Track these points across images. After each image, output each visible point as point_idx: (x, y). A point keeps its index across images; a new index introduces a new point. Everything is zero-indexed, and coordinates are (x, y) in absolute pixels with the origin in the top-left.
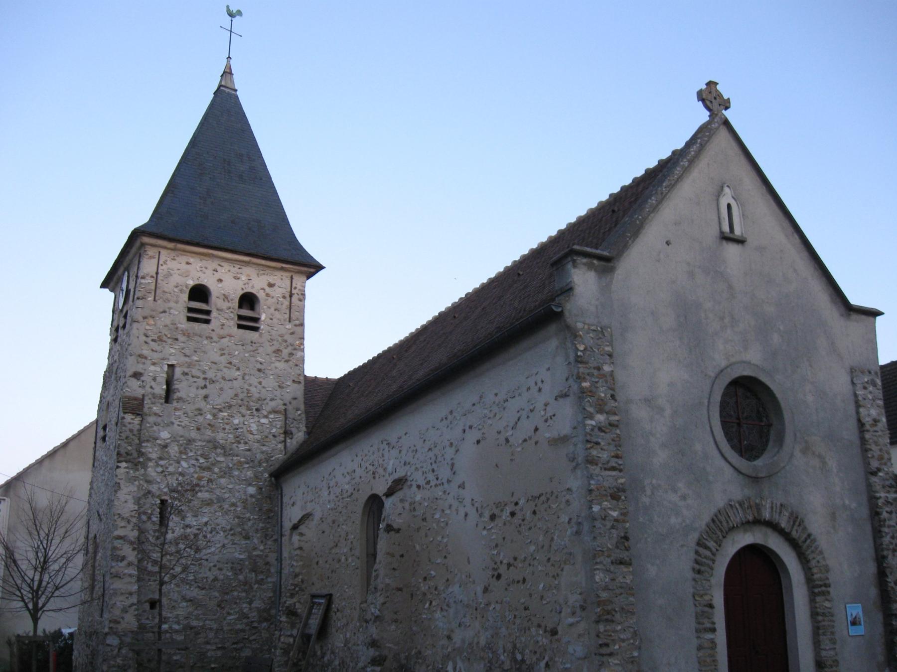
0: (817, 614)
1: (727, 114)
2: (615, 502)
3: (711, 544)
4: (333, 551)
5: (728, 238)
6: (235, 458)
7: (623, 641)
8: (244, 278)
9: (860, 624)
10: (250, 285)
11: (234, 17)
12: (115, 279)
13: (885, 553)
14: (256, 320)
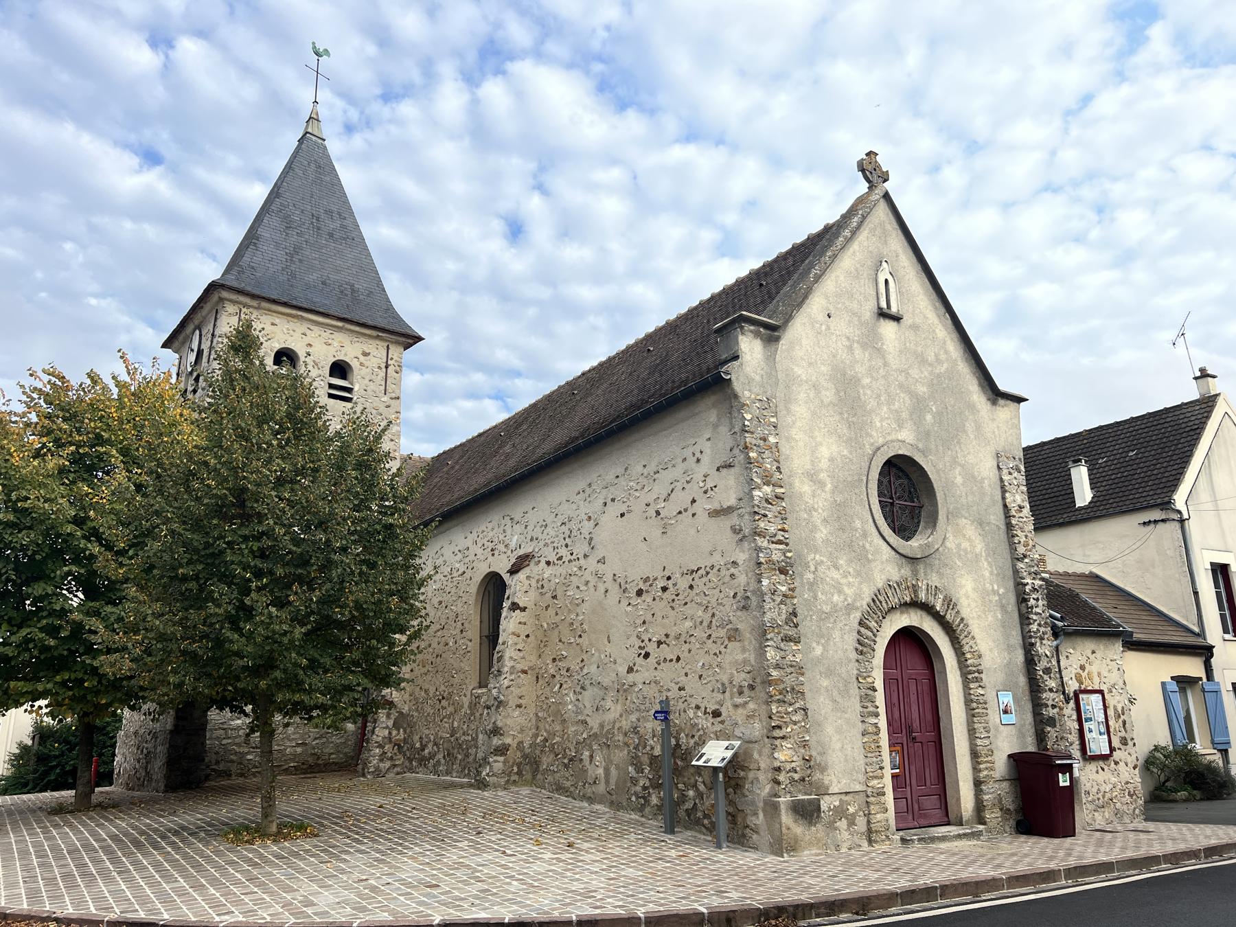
1: (887, 186)
2: (783, 577)
3: (873, 624)
4: (439, 633)
5: (884, 314)
7: (795, 723)
12: (181, 338)
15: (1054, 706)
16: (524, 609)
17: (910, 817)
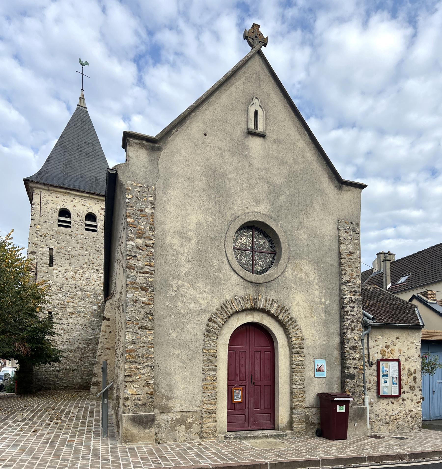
0: (293, 364)
3: (219, 321)
6: (86, 293)
7: (143, 374)
8: (87, 205)
9: (323, 371)
10: (91, 209)
11: (84, 66)
13: (345, 331)
14: (96, 226)
15: (355, 368)
16: (109, 319)
17: (247, 425)
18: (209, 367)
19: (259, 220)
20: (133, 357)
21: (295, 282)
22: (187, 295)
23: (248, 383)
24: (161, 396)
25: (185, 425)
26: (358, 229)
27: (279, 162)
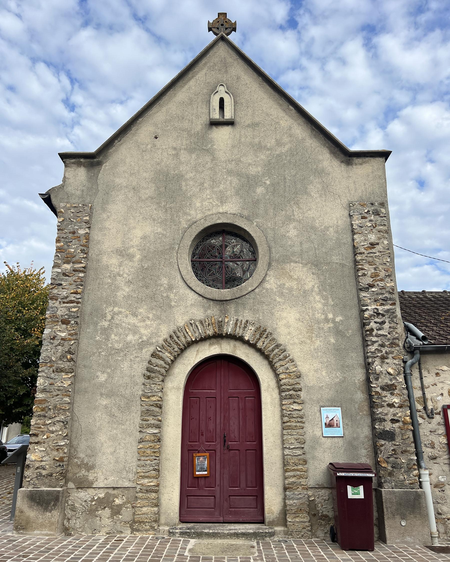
2: (64, 326)
3: (167, 356)
7: (53, 432)
9: (338, 426)
13: (370, 360)
15: (393, 421)
17: (217, 513)
18: (149, 422)
19: (225, 221)
20: (43, 410)
21: (282, 295)
22: (124, 324)
23: (218, 446)
24: (79, 463)
25: (111, 508)
26: (383, 210)
27: (255, 148)
